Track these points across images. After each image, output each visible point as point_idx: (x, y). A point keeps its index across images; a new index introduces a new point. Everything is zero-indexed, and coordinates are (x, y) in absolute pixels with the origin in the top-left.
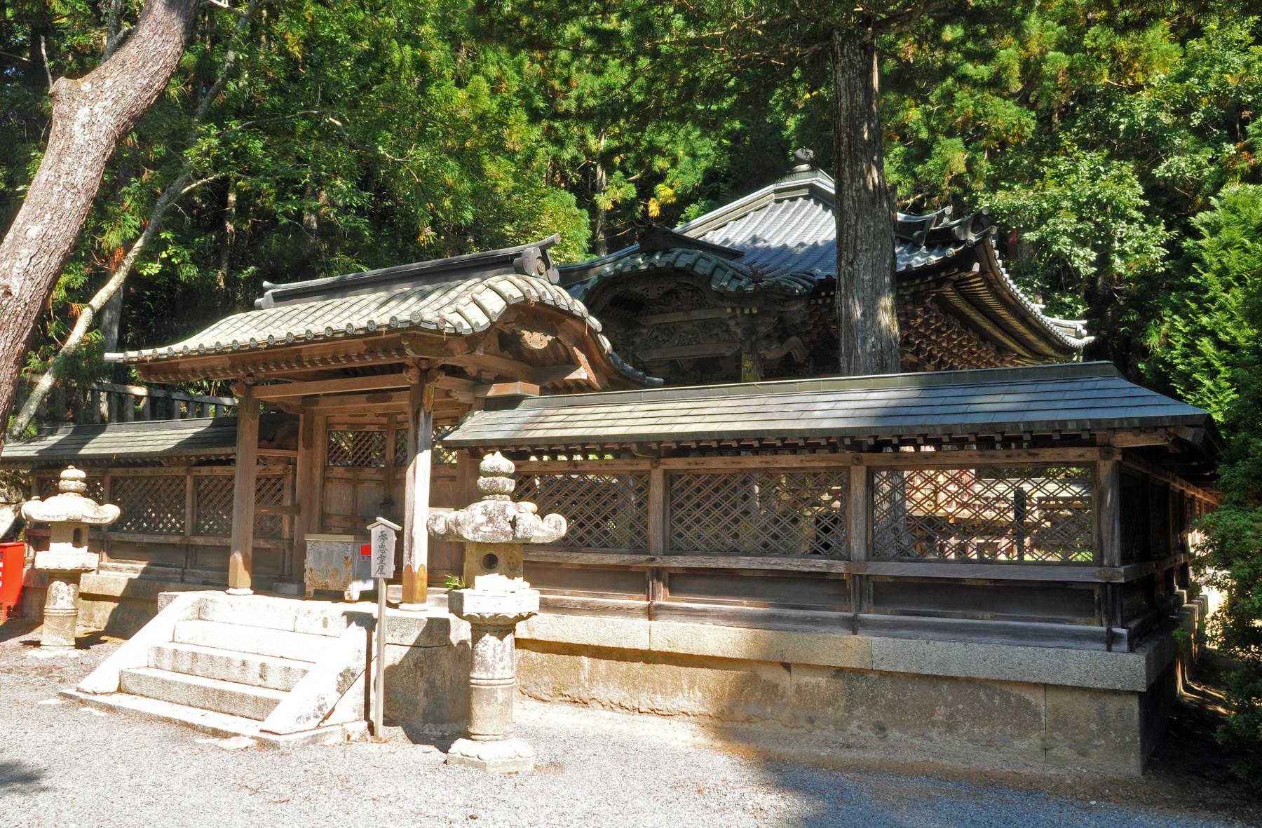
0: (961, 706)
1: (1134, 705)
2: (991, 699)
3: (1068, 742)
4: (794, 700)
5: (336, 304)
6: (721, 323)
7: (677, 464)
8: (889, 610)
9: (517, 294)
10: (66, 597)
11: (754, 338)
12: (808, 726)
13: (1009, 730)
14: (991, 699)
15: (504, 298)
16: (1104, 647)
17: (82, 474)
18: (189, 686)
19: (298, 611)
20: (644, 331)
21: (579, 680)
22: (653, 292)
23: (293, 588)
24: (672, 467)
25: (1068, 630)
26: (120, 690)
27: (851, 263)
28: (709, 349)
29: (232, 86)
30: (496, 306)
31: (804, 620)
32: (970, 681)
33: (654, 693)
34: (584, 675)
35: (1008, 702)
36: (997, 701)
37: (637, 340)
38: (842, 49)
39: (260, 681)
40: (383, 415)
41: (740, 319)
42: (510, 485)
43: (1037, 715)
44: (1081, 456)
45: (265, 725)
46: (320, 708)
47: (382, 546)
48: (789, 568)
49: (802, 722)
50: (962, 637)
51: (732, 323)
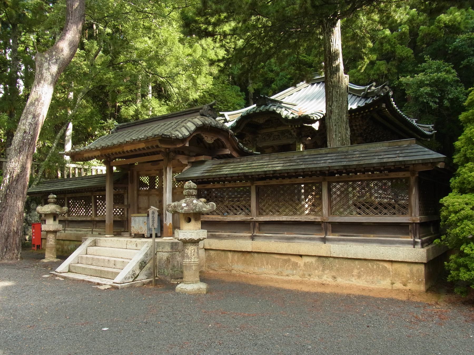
0: (362, 269)
1: (422, 268)
2: (373, 266)
3: (400, 281)
4: (303, 268)
5: (137, 130)
6: (288, 131)
7: (260, 183)
8: (337, 234)
9: (200, 123)
10: (53, 241)
11: (301, 136)
12: (309, 277)
13: (379, 277)
14: (373, 266)
15: (195, 125)
16: (412, 246)
17: (55, 196)
18: (91, 269)
19: (127, 241)
20: (260, 136)
21: (228, 263)
22: (261, 121)
23: (127, 234)
24: (258, 184)
25: (400, 240)
26: (69, 271)
27: (331, 106)
28: (284, 141)
29: (152, 34)
30: (193, 128)
31: (306, 239)
32: (365, 260)
33: (254, 266)
34: (229, 261)
35: (379, 267)
36: (375, 267)
37: (258, 139)
38: (327, 25)
39: (114, 267)
40: (157, 170)
41: (295, 129)
42: (195, 192)
43: (389, 272)
44: (404, 175)
45: (115, 281)
46: (133, 275)
47: (153, 217)
48: (301, 220)
49: (307, 276)
50: (363, 244)
51: (292, 131)
